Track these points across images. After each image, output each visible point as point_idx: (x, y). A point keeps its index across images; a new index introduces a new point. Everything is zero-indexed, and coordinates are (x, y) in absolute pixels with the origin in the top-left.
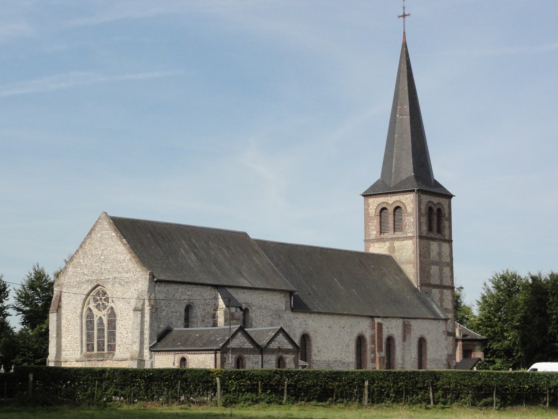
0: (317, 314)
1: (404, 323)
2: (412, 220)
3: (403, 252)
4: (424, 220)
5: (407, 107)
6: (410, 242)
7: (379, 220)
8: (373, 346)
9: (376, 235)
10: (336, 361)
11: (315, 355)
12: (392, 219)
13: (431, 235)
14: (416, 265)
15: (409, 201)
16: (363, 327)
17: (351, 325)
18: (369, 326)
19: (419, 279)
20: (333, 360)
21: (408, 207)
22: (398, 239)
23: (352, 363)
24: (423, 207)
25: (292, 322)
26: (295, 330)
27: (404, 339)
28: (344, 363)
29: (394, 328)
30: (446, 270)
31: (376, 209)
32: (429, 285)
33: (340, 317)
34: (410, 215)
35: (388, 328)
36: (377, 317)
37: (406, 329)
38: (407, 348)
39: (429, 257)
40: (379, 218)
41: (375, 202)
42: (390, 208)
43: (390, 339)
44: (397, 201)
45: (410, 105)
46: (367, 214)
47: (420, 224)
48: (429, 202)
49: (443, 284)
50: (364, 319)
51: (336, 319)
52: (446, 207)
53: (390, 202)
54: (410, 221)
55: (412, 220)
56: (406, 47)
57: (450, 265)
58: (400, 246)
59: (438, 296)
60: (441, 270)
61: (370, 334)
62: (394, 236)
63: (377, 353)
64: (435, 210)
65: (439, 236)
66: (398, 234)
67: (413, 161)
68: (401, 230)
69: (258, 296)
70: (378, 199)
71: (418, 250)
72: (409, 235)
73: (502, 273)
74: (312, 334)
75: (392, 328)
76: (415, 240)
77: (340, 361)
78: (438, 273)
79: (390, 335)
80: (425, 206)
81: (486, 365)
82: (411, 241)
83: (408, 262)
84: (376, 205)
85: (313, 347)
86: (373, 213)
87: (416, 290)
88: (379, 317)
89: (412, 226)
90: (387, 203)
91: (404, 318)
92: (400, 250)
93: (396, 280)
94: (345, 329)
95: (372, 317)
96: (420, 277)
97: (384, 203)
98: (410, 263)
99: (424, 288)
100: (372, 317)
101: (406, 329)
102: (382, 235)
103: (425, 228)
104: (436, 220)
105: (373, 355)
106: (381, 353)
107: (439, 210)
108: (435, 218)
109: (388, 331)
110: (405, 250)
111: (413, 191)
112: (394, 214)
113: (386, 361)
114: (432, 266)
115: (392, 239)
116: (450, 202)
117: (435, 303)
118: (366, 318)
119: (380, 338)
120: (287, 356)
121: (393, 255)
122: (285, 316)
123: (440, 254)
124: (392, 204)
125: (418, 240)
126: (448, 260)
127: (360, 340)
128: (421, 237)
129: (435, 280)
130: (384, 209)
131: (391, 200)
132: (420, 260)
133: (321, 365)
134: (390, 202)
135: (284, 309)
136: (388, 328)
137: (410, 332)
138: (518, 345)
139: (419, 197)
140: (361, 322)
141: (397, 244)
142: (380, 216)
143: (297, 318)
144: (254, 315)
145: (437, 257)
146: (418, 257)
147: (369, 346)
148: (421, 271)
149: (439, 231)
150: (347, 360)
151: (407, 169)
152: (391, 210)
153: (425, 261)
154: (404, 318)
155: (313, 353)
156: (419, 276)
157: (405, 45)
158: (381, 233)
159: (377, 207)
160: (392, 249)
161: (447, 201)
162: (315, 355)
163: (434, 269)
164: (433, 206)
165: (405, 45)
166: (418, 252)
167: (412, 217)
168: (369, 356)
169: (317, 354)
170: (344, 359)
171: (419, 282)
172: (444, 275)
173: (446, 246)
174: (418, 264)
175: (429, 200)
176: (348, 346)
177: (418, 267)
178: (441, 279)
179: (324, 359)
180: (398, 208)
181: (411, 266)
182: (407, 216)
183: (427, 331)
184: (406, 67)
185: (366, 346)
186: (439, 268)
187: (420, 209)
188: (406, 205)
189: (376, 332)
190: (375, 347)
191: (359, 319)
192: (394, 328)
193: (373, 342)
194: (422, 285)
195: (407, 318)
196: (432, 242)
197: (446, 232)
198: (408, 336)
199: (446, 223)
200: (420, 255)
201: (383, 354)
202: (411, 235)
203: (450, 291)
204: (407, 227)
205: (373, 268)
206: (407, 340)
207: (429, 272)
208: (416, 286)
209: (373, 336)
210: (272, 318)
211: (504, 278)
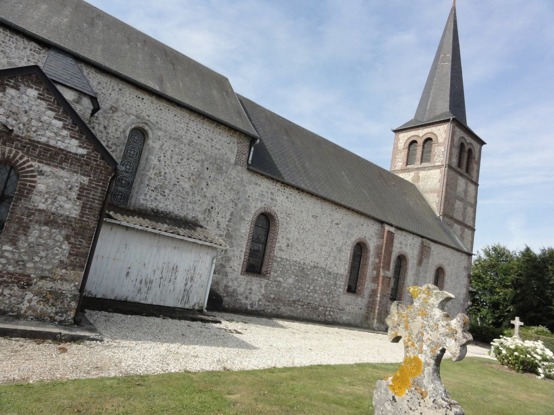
0: (297, 192)
1: (422, 243)
2: (443, 150)
3: (427, 182)
4: (456, 152)
5: (449, 56)
6: (438, 171)
7: (406, 152)
8: (377, 260)
9: (402, 166)
10: (315, 267)
11: (281, 250)
12: (421, 150)
13: (459, 169)
14: (441, 194)
15: (442, 133)
16: (369, 232)
17: (350, 224)
18: (376, 234)
19: (442, 208)
20: (312, 264)
21: (439, 138)
22: (424, 169)
23: (342, 275)
24: (456, 139)
25: (245, 186)
26: (247, 200)
27: (420, 263)
28: (329, 273)
29: (409, 246)
30: (470, 210)
31: (405, 143)
32: (452, 218)
33: (334, 207)
34: (440, 145)
35: (401, 243)
36: (388, 224)
37: (424, 253)
38: (422, 274)
39: (456, 191)
40: (407, 150)
41: (404, 137)
42: (420, 140)
43: (402, 259)
44: (429, 133)
45: (453, 53)
46: (396, 147)
47: (451, 154)
48: (463, 138)
49: (465, 223)
50: (371, 222)
51: (328, 208)
52: (477, 150)
53: (421, 135)
54: (441, 153)
55: (443, 150)
56: (455, 11)
57: (474, 206)
58: (426, 175)
59: (459, 233)
60: (465, 209)
61: (375, 244)
62: (420, 166)
63: (381, 270)
64: (467, 148)
65: (466, 174)
66: (425, 164)
67: (450, 100)
68: (428, 160)
69: (176, 119)
70: (408, 133)
71: (445, 178)
72: (437, 164)
73: (493, 245)
74: (280, 216)
75: (406, 245)
76: (443, 169)
77: (324, 269)
78: (462, 210)
79: (403, 253)
80: (458, 139)
81: (475, 312)
82: (439, 171)
83: (432, 191)
84: (406, 138)
85: (279, 237)
86: (402, 146)
87: (438, 219)
88: (391, 225)
89: (441, 156)
90: (418, 136)
91: (422, 237)
92: (425, 179)
93: (417, 203)
94: (340, 226)
95: (382, 222)
96: (444, 206)
97: (414, 136)
98: (434, 192)
99: (447, 220)
100: (382, 222)
101: (424, 253)
102: (408, 166)
103: (455, 161)
104: (466, 157)
105: (375, 272)
106: (387, 272)
107: (470, 151)
108: (466, 155)
109: (401, 248)
110: (431, 181)
111: (448, 121)
112: (423, 146)
113: (392, 284)
114: (457, 201)
115: (418, 169)
116: (481, 149)
117: (457, 236)
118: (372, 222)
119: (389, 252)
120: (46, 168)
121: (416, 184)
122: (234, 173)
123: (466, 192)
124: (423, 136)
125: (446, 169)
126: (473, 201)
127: (360, 249)
128: (450, 167)
129: (458, 216)
130: (414, 142)
131: (422, 133)
132: (446, 190)
133: (288, 267)
134: (421, 135)
135: (233, 161)
136: (401, 243)
137: (428, 257)
138: (507, 301)
139: (453, 128)
140: (365, 225)
141: (422, 174)
142: (409, 148)
143: (256, 184)
144: (157, 145)
145: (463, 194)
146: (445, 186)
147: (371, 259)
148: (445, 201)
149: (467, 170)
150: (335, 270)
151: (443, 106)
152: (420, 142)
153: (450, 195)
154: (422, 237)
155: (277, 245)
156: (442, 205)
157: (454, 9)
158: (407, 164)
159: (406, 141)
160: (418, 178)
161: (479, 146)
162: (281, 250)
163: (458, 204)
164: (465, 144)
165: (454, 9)
166: (445, 180)
167: (442, 147)
168: (369, 271)
169: (284, 247)
170: (330, 268)
171: (442, 211)
172: (467, 214)
173: (472, 187)
174: (444, 193)
175: (463, 136)
176: (340, 250)
177: (443, 196)
178: (464, 218)
179: (295, 259)
180: (429, 139)
181: (435, 195)
182: (438, 146)
183: (447, 261)
184: (453, 24)
185: (367, 258)
186: (464, 205)
187: (452, 140)
188: (438, 135)
189: (385, 242)
190: (380, 262)
191: (362, 220)
192: (409, 246)
193: (378, 255)
194: (445, 215)
195: (427, 239)
196: (460, 177)
197: (474, 174)
198: (425, 260)
199: (475, 166)
200: (447, 185)
201: (390, 273)
202: (440, 164)
203: (470, 232)
204: (436, 157)
205: (394, 185)
206: (423, 264)
207: (453, 205)
208: (438, 215)
209: (379, 248)
210: (202, 166)
211: (495, 249)
